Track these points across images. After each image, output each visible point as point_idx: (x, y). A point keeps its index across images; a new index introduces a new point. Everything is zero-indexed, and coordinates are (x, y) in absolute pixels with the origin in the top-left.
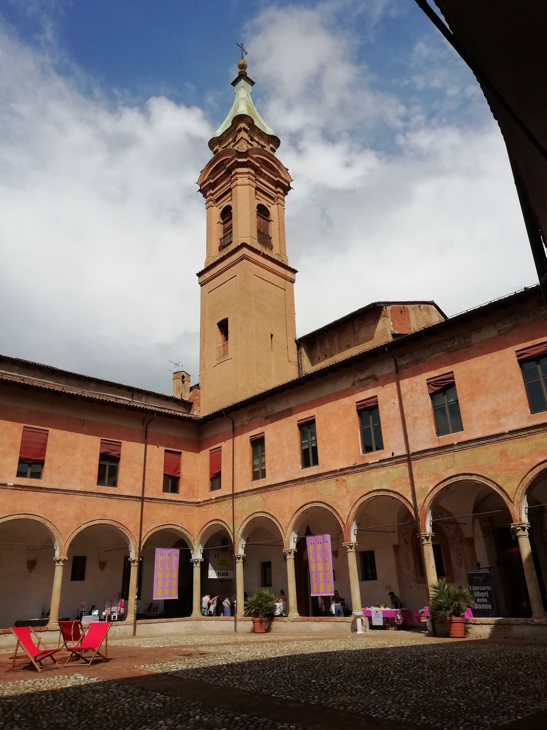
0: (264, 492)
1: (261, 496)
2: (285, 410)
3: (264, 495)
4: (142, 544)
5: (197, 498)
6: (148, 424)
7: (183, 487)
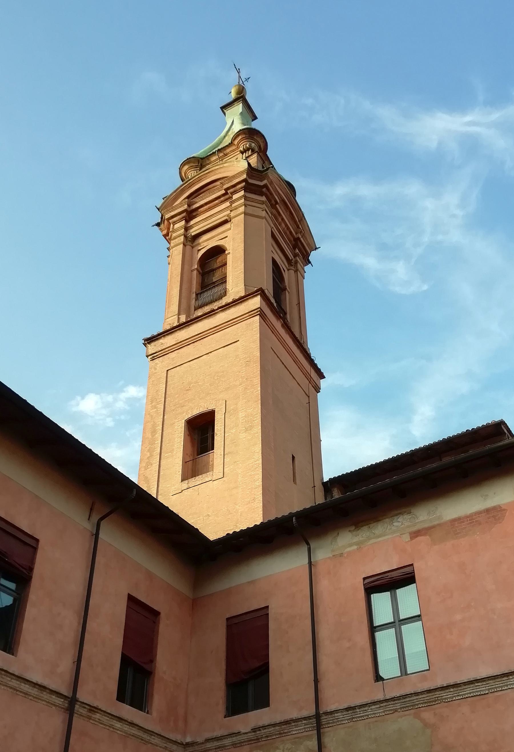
0: (429, 704)
1: (417, 716)
2: (479, 513)
3: (427, 715)
4: (273, 300)
5: (184, 734)
6: (102, 519)
7: (158, 701)
